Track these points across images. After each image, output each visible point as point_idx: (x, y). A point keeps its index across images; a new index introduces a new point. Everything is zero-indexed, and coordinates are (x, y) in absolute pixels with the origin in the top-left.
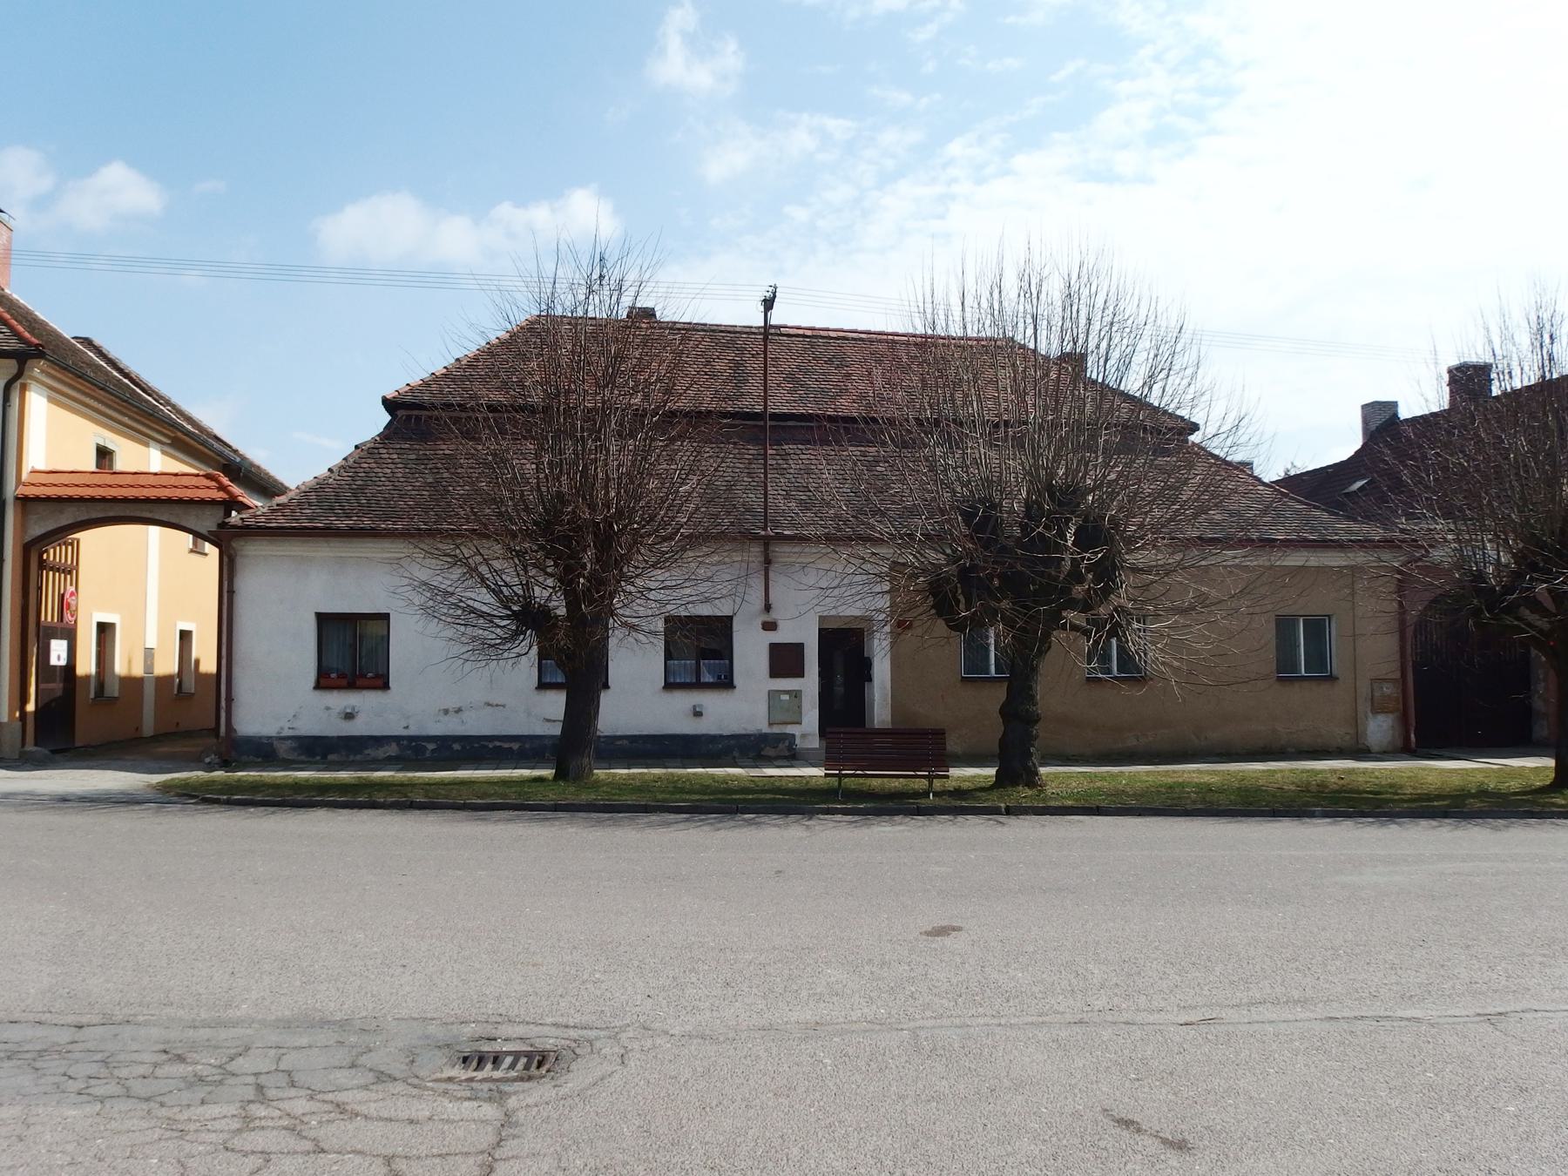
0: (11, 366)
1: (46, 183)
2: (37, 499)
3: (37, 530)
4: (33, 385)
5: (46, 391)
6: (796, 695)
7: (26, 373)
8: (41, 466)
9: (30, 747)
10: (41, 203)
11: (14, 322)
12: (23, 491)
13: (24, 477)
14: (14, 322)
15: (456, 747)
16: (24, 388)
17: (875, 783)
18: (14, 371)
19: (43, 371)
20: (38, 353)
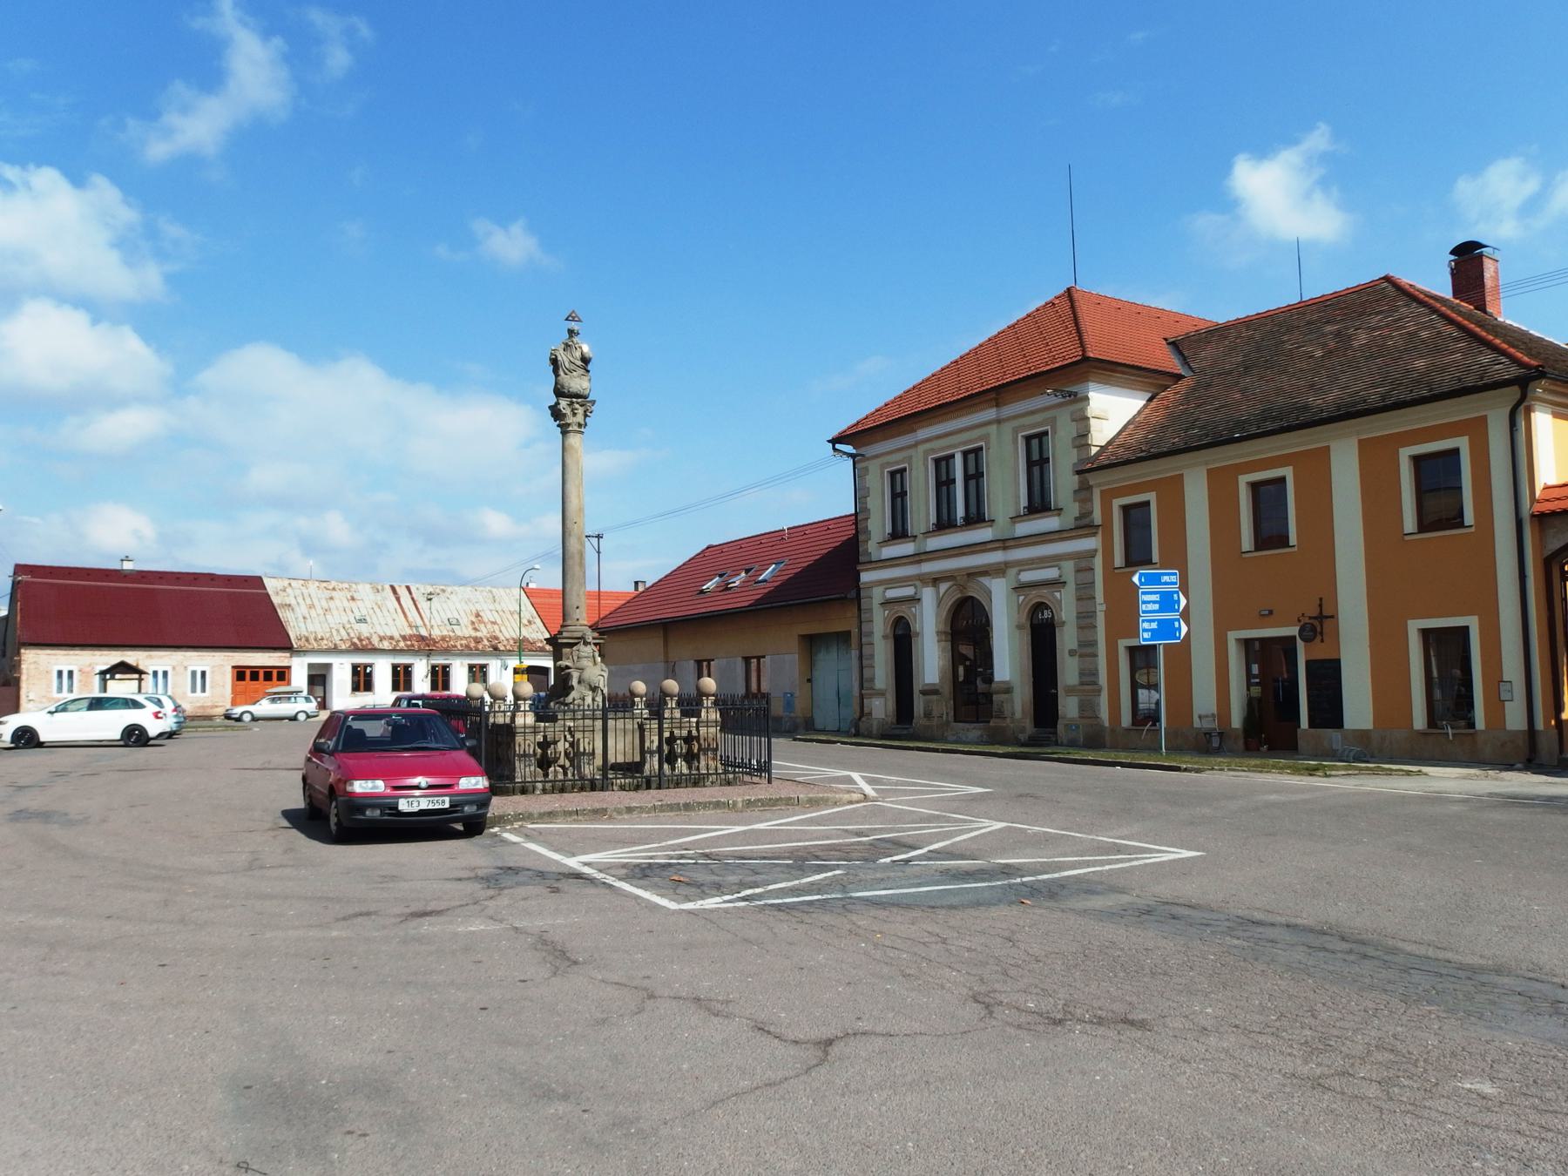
0: (1513, 392)
1: (1532, 186)
2: (1553, 513)
3: (1555, 544)
4: (1537, 405)
5: (1550, 408)
6: (1158, 749)
7: (1530, 395)
8: (1553, 481)
9: (1462, 443)
10: (1531, 207)
11: (1512, 350)
12: (1538, 508)
13: (1538, 493)
14: (1512, 350)
15: (1255, 669)
16: (1529, 411)
17: (1512, 668)
18: (1518, 396)
19: (1545, 390)
20: (1539, 374)
